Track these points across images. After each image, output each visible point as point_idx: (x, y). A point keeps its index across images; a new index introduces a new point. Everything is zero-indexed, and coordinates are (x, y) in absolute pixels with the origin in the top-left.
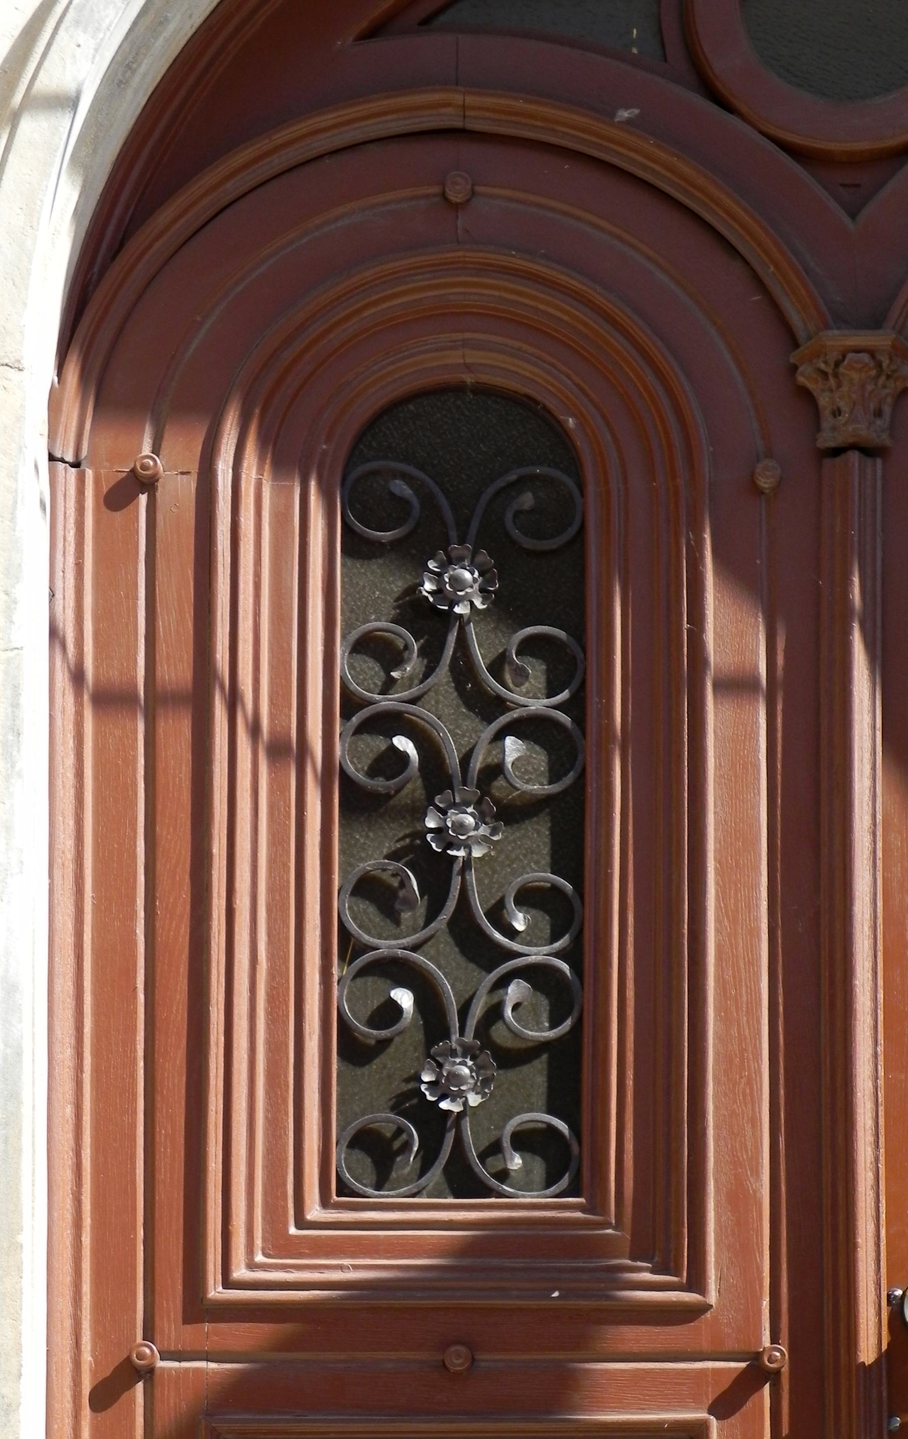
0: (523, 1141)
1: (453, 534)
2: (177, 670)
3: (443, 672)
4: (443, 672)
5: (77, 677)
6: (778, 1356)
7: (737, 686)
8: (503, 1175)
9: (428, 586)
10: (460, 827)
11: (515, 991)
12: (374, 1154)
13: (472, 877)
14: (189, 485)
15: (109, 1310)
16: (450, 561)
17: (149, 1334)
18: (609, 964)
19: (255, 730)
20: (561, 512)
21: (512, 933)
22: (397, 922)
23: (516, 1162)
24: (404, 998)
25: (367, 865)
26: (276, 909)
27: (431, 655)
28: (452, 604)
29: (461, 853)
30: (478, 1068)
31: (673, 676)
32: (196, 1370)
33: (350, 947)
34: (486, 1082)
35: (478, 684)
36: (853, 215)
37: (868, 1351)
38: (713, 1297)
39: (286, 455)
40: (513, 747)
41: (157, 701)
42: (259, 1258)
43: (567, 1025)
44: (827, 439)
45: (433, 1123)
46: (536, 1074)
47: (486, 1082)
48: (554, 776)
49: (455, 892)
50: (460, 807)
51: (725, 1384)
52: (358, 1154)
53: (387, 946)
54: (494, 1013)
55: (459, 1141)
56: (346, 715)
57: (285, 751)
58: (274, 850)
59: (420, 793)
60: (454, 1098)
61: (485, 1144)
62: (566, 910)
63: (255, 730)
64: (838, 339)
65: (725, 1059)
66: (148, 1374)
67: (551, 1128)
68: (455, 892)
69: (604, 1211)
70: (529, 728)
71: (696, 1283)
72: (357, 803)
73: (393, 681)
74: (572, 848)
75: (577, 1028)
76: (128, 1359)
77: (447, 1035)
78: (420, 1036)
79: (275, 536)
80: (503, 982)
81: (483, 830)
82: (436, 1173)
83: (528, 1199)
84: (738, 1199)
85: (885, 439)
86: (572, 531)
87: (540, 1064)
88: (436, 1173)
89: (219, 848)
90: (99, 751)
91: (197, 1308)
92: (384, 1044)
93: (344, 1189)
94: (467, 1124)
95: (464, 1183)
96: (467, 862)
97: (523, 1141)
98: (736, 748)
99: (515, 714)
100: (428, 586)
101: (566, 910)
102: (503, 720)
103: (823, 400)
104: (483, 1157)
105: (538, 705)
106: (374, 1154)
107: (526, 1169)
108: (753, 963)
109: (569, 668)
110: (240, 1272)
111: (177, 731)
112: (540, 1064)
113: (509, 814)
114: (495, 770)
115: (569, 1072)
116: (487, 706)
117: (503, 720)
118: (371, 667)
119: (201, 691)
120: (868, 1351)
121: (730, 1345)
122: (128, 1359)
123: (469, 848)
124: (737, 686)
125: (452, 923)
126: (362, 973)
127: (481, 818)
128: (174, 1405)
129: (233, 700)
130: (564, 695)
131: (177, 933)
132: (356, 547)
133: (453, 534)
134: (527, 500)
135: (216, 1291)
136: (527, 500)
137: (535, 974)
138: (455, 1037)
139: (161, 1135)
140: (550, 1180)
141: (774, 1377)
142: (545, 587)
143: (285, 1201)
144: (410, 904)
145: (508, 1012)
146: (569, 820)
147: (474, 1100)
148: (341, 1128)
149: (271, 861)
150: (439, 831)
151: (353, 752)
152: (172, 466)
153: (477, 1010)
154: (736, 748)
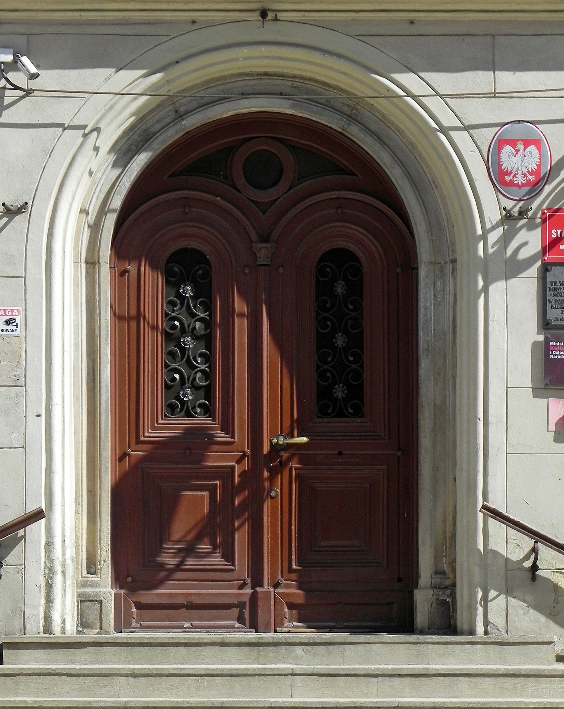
0: (200, 406)
1: (186, 279)
2: (133, 312)
3: (184, 308)
4: (184, 308)
5: (115, 314)
6: (249, 452)
7: (241, 315)
8: (196, 413)
9: (181, 290)
10: (188, 341)
11: (199, 375)
12: (172, 408)
13: (190, 351)
14: (135, 272)
15: (122, 442)
16: (186, 285)
17: (129, 447)
18: (216, 391)
19: (148, 324)
20: (207, 275)
21: (197, 363)
22: (175, 360)
23: (199, 410)
24: (177, 376)
25: (170, 349)
26: (153, 358)
27: (182, 304)
28: (186, 294)
29: (188, 347)
30: (191, 391)
31: (229, 314)
32: (137, 454)
33: (167, 366)
34: (193, 394)
35: (191, 310)
36: (264, 214)
37: (265, 451)
38: (236, 440)
39: (154, 266)
40: (198, 324)
41: (130, 319)
42: (150, 431)
43: (207, 383)
44: (258, 263)
45: (183, 402)
46: (202, 392)
47: (193, 394)
48: (206, 331)
49: (187, 355)
50: (188, 337)
51: (239, 457)
52: (168, 408)
53: (174, 365)
54: (194, 379)
55: (188, 406)
56: (166, 317)
57: (154, 328)
58: (153, 345)
59: (180, 333)
60: (186, 397)
61: (193, 406)
62: (208, 359)
63: (148, 324)
64: (260, 245)
65: (238, 390)
66: (128, 272)
67: (205, 403)
68: (187, 355)
69: (215, 421)
70: (201, 320)
71: (233, 437)
72: (168, 337)
73: (174, 310)
74: (209, 346)
75: (211, 331)
76: (125, 452)
77: (185, 384)
78: (180, 384)
79: (153, 281)
80: (196, 373)
81: (192, 341)
82: (183, 412)
83: (201, 420)
84: (241, 419)
85: (270, 263)
86: (209, 279)
87: (203, 389)
88: (183, 412)
89: (141, 412)
90: (119, 327)
91: (138, 442)
92: (173, 386)
93: (166, 416)
94: (189, 403)
95: (188, 415)
96: (189, 348)
97: (200, 406)
98: (241, 327)
99: (198, 317)
100: (181, 290)
101: (208, 359)
102: (196, 318)
103: (258, 256)
104: (192, 409)
105: (202, 315)
106: (172, 408)
107: (201, 412)
108: (244, 371)
109: (208, 307)
110: (146, 434)
111: (134, 324)
112: (203, 389)
113: (196, 338)
114: (194, 328)
115: (208, 392)
116: (193, 315)
117: (196, 318)
118: (170, 307)
119: (139, 316)
120: (265, 451)
121: (240, 449)
122: (125, 452)
123: (189, 345)
124: (241, 315)
125: (186, 361)
126: (169, 371)
127: (192, 339)
128: (133, 460)
129: (144, 318)
130: (208, 415)
131: (134, 364)
132: (168, 282)
133: (186, 279)
134: (200, 272)
135: (142, 438)
136: (200, 272)
137: (203, 371)
138: (187, 384)
139: (131, 406)
140: (205, 414)
141: (248, 456)
142: (204, 294)
143: (154, 420)
144: (178, 356)
145: (197, 380)
146: (207, 340)
147: (190, 398)
148: (165, 403)
149: (152, 349)
150: (184, 342)
151: (167, 325)
152: (132, 268)
153: (191, 379)
154: (241, 327)
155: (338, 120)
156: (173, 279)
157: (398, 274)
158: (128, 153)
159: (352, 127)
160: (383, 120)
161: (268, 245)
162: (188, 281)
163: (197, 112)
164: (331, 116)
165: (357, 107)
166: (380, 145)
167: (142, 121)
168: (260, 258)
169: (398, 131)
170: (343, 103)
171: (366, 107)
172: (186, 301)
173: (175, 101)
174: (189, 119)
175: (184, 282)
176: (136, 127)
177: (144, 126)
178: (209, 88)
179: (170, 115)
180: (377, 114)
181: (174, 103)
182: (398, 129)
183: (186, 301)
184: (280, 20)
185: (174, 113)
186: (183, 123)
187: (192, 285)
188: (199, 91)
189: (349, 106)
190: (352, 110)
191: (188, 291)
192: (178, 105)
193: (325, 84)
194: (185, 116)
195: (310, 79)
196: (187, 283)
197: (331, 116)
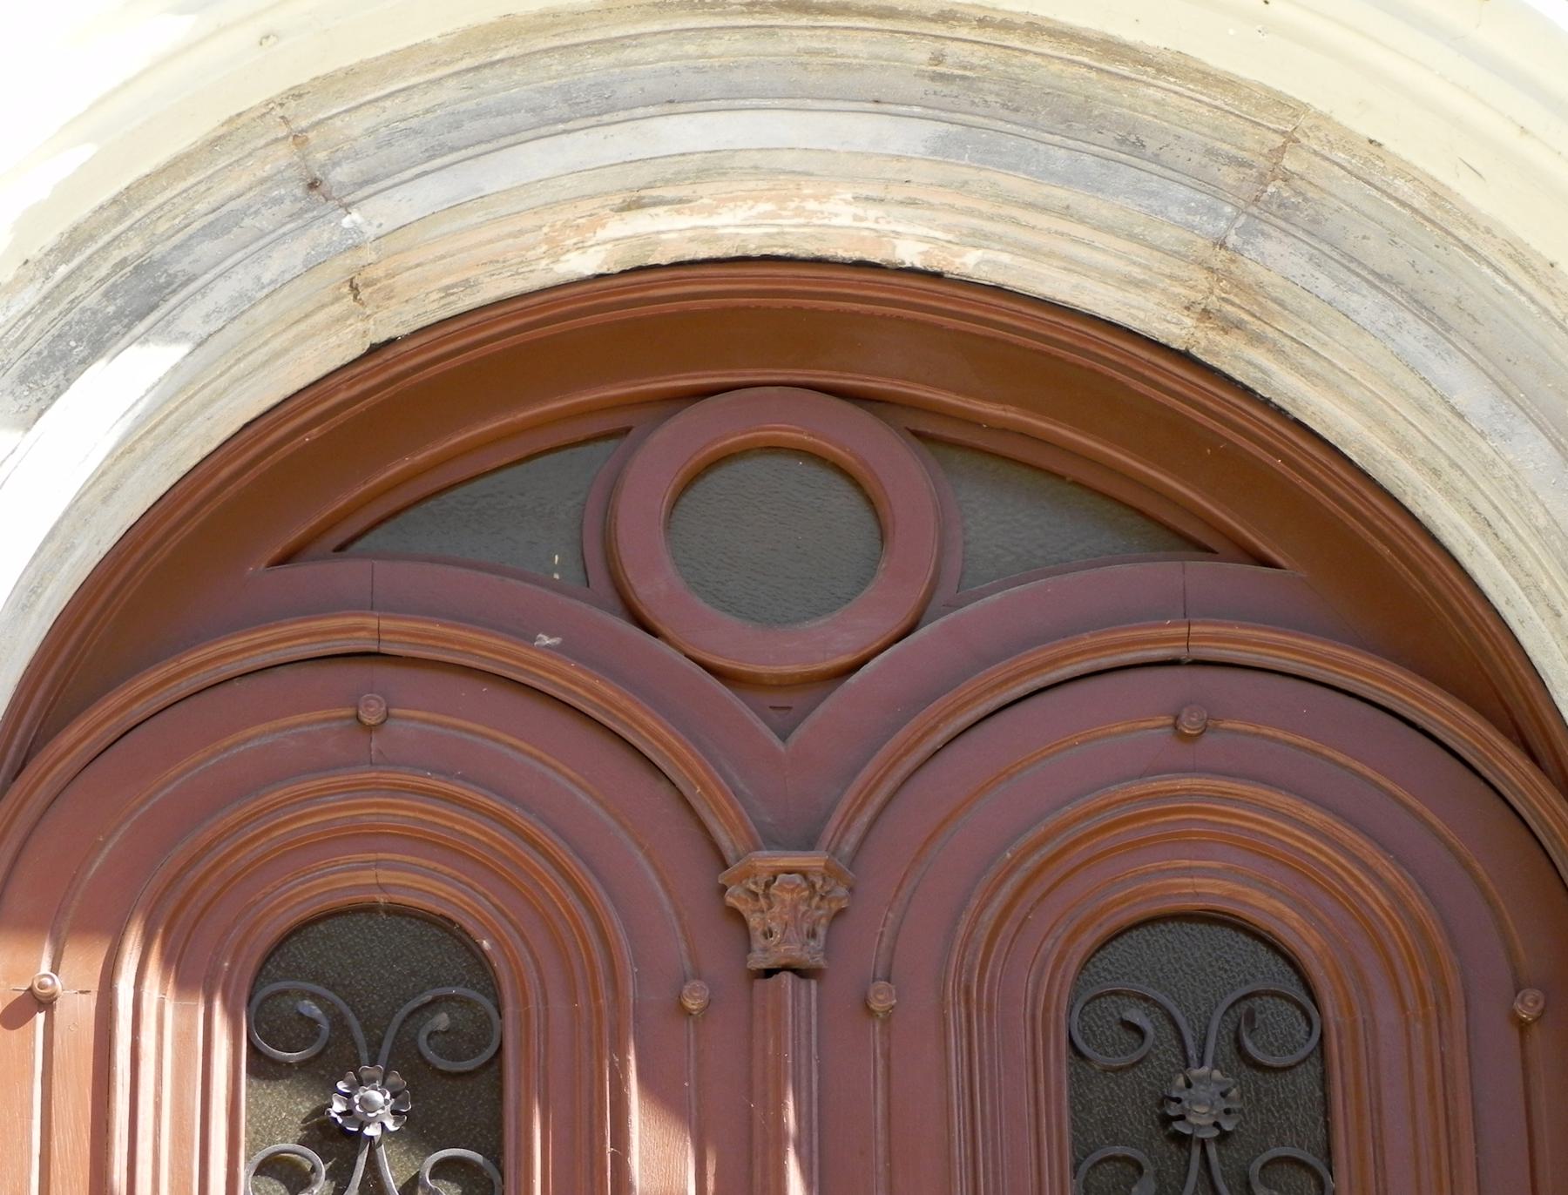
1: (364, 1055)
16: (360, 1083)
36: (783, 738)
39: (189, 974)
44: (758, 961)
64: (768, 859)
85: (819, 961)
103: (754, 921)
132: (261, 1066)
134: (442, 1020)
136: (442, 1020)
155: (1189, 211)
156: (294, 1057)
157: (1523, 1026)
158: (47, 373)
159: (1269, 247)
160: (1438, 215)
161: (813, 860)
162: (373, 1063)
163: (425, 173)
164: (1152, 194)
165: (1289, 163)
166: (1425, 330)
167: (124, 214)
168: (768, 934)
169: (1526, 268)
170: (1211, 152)
171: (1340, 156)
172: (362, 1161)
173: (304, 124)
174: (377, 204)
175: (355, 1066)
176: (92, 238)
177: (134, 247)
178: (492, 64)
179: (279, 201)
180: (1404, 188)
181: (299, 138)
182: (1519, 256)
183: (362, 1161)
184: (751, 988)
185: (299, 192)
186: (346, 222)
187: (395, 1078)
188: (439, 81)
189: (1242, 164)
190: (1262, 179)
191: (378, 1107)
192: (321, 156)
193: (1111, 48)
194: (360, 194)
195: (1034, 28)
196: (366, 1070)
197: (1152, 194)
